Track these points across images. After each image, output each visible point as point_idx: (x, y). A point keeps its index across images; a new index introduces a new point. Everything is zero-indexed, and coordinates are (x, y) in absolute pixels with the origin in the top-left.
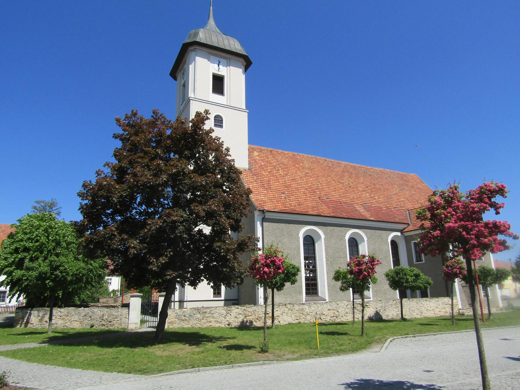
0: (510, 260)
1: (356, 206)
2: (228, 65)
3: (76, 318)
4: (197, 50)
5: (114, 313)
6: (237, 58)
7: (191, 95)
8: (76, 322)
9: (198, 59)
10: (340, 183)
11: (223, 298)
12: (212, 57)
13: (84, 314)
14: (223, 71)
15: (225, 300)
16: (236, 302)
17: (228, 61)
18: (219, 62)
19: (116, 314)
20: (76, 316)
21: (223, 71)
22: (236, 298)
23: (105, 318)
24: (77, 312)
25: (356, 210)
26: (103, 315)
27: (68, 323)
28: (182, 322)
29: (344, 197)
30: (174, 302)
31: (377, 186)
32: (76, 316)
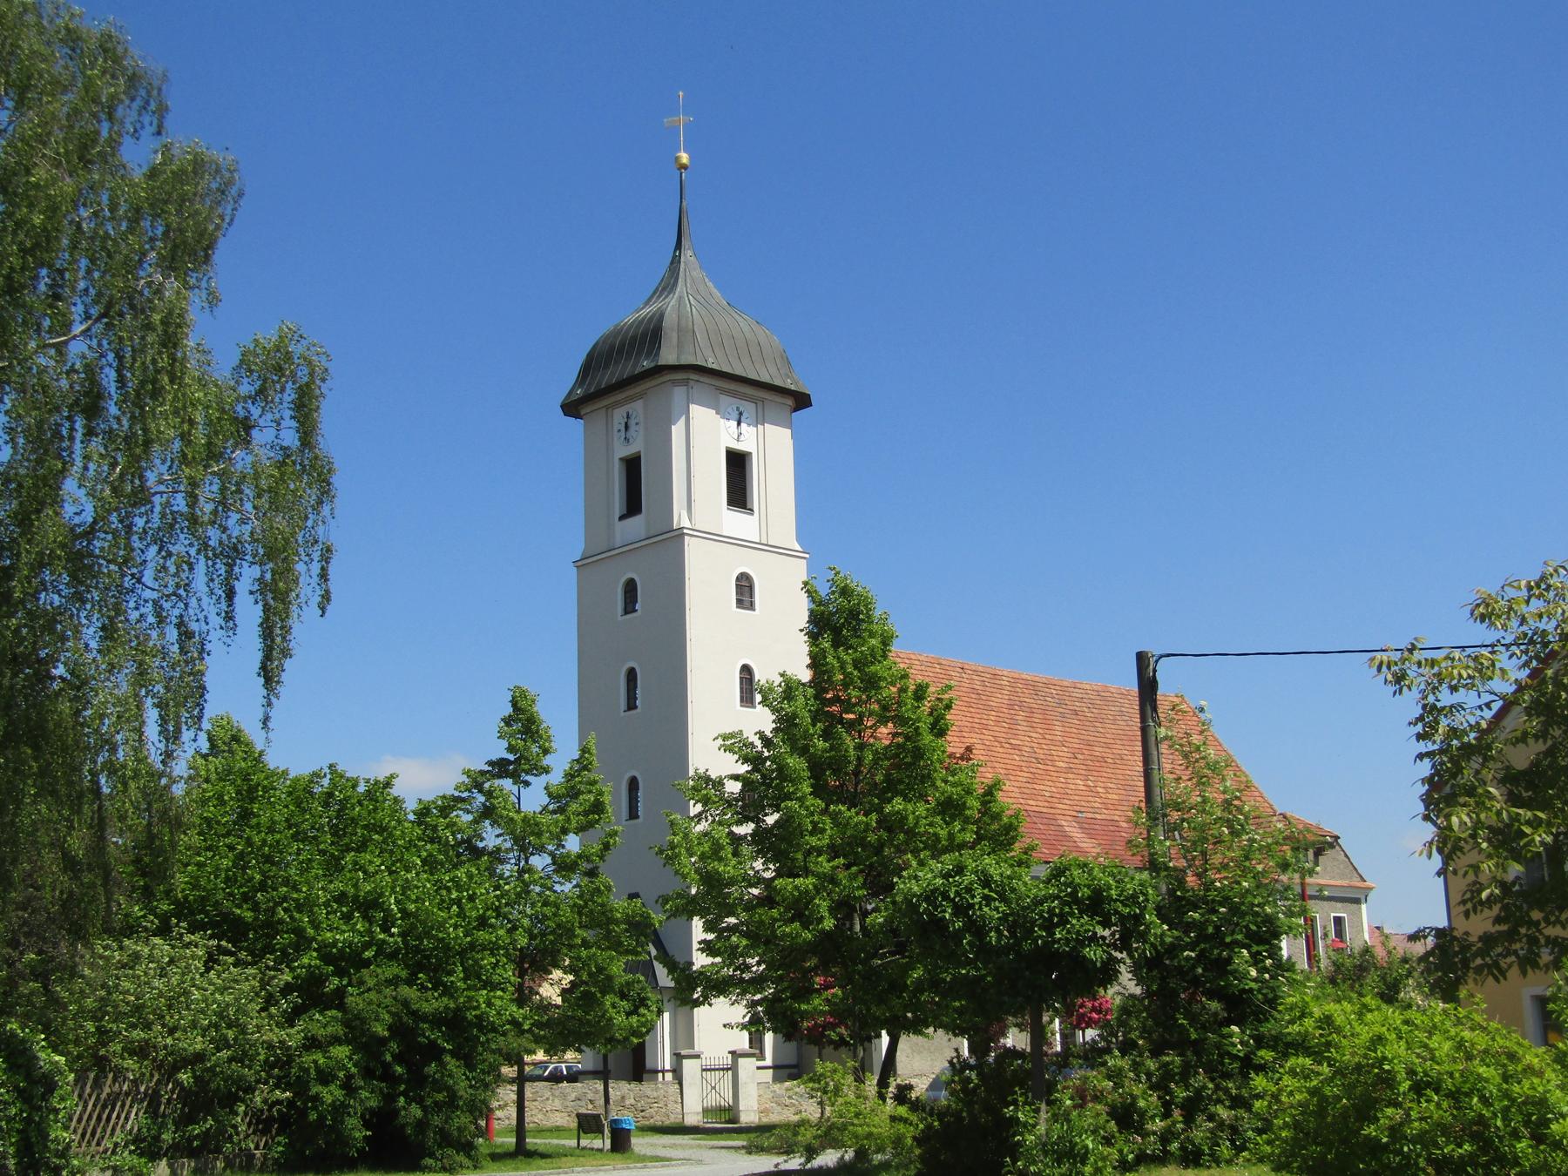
0: (251, 593)
1: (1064, 823)
2: (759, 420)
3: (557, 1104)
4: (692, 383)
5: (649, 1093)
6: (778, 399)
7: (680, 518)
8: (557, 1114)
9: (696, 410)
10: (1014, 747)
11: (769, 1061)
12: (725, 400)
13: (573, 1095)
14: (748, 439)
15: (775, 1067)
16: (794, 1071)
17: (760, 404)
18: (741, 414)
19: (655, 1094)
20: (556, 1100)
21: (748, 439)
22: (793, 1061)
23: (627, 1102)
24: (557, 1093)
25: (1067, 837)
26: (623, 1098)
27: (540, 1116)
28: (785, 1111)
29: (1033, 796)
30: (663, 1071)
31: (1098, 751)
32: (556, 1100)
